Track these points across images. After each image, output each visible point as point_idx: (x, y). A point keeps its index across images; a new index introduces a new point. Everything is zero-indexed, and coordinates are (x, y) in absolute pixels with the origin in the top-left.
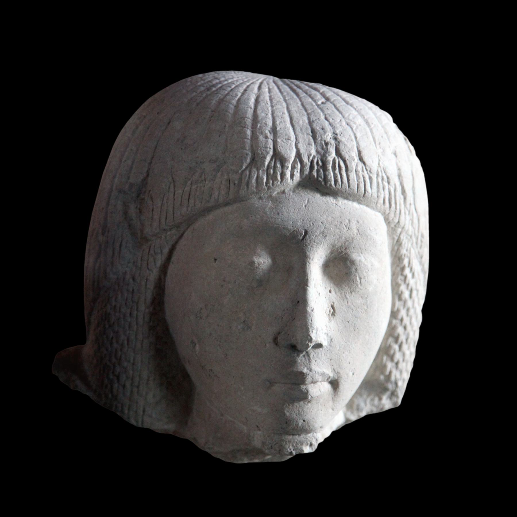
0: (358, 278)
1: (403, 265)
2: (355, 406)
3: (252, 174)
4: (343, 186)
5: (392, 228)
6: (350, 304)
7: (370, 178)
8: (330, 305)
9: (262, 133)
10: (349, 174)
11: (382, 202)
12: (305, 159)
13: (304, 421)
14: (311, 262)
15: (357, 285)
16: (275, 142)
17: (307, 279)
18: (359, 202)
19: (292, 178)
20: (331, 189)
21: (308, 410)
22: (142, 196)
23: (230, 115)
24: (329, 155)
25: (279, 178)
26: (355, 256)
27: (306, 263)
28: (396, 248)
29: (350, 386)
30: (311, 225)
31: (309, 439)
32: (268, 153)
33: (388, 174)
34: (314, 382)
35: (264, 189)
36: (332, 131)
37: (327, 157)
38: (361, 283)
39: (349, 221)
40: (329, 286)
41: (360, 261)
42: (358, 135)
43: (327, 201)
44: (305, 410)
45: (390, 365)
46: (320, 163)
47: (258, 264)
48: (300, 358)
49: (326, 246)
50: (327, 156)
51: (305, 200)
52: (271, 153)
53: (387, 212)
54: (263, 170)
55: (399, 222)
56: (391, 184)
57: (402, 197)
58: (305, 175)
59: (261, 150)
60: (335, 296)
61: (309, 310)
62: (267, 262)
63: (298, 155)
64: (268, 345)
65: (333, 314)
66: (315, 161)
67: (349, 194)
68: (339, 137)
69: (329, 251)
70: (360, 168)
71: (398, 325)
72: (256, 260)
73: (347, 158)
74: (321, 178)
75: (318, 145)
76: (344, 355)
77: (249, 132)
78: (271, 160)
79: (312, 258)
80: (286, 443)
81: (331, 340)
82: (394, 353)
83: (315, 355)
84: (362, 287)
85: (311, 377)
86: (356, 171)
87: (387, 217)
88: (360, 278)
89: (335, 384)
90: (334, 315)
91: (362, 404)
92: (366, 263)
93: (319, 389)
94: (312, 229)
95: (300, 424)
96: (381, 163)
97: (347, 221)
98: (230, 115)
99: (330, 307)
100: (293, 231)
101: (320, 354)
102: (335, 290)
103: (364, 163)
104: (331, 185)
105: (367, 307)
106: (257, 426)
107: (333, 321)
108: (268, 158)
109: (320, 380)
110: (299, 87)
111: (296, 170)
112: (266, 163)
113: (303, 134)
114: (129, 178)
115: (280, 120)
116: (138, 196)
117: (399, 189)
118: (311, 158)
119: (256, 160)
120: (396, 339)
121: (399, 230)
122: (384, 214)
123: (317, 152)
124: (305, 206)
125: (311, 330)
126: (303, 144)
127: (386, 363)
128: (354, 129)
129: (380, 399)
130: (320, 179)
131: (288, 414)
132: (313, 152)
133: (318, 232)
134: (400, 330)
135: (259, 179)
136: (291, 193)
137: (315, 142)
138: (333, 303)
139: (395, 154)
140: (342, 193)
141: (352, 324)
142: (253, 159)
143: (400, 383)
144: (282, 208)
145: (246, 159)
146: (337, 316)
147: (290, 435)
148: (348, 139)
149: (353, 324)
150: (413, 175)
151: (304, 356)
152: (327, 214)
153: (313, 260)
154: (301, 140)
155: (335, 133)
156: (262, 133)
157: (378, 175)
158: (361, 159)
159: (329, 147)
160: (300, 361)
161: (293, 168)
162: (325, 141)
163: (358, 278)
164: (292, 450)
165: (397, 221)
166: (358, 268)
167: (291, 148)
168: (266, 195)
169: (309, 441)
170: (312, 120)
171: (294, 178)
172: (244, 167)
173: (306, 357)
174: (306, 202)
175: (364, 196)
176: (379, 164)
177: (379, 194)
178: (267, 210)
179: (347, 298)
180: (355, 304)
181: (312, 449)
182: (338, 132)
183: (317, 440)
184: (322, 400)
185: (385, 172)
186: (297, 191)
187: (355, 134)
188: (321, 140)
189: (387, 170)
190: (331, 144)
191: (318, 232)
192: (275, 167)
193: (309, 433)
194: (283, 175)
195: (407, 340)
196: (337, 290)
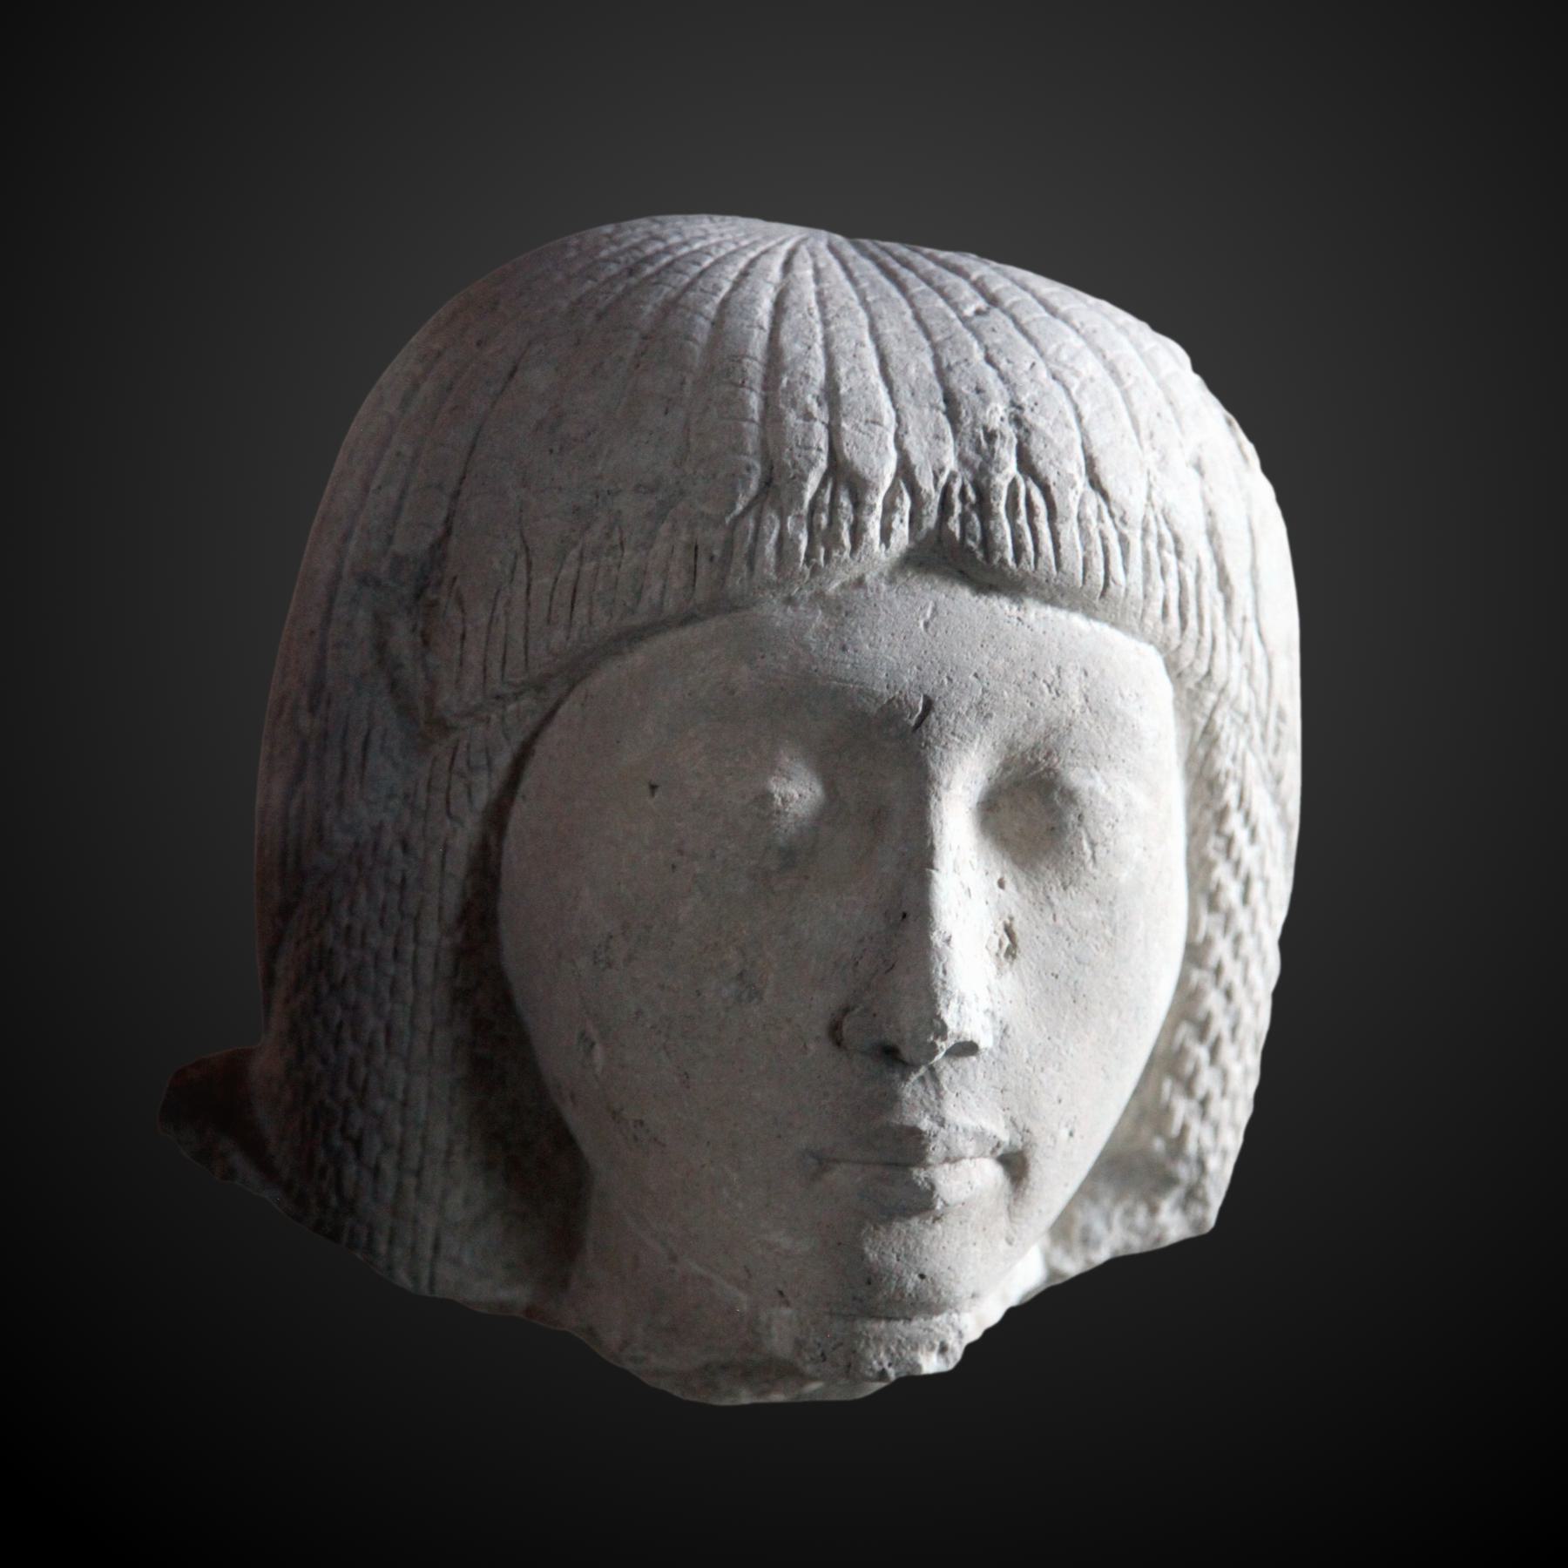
0: (1085, 844)
1: (1222, 804)
2: (1076, 1233)
3: (766, 528)
4: (1041, 565)
5: (1190, 691)
6: (1060, 921)
7: (1123, 540)
8: (1000, 924)
9: (794, 404)
10: (1060, 527)
11: (1159, 612)
12: (926, 483)
13: (922, 1276)
14: (944, 794)
15: (1083, 863)
16: (834, 431)
17: (932, 847)
18: (1090, 612)
19: (885, 540)
20: (1004, 574)
21: (935, 1245)
22: (430, 595)
23: (698, 350)
24: (998, 471)
25: (846, 539)
26: (1075, 777)
27: (928, 798)
28: (1201, 752)
29: (1062, 1172)
30: (942, 684)
31: (937, 1330)
32: (812, 464)
33: (1176, 529)
34: (952, 1159)
35: (802, 574)
36: (1007, 398)
37: (990, 477)
38: (1093, 857)
39: (1059, 669)
40: (999, 866)
41: (1092, 791)
42: (1086, 410)
43: (992, 610)
44: (925, 1243)
45: (1182, 1108)
46: (971, 495)
47: (784, 800)
48: (909, 1085)
49: (989, 747)
50: (993, 472)
51: (926, 606)
52: (823, 464)
53: (1175, 642)
54: (799, 516)
55: (1209, 673)
56: (1185, 557)
57: (1219, 597)
58: (924, 530)
59: (791, 456)
60: (1017, 897)
61: (937, 939)
62: (808, 794)
63: (905, 471)
64: (812, 1047)
65: (1011, 953)
66: (956, 488)
67: (1058, 588)
68: (1028, 415)
69: (997, 762)
70: (1090, 511)
71: (1209, 986)
72: (777, 787)
73: (1053, 478)
74: (974, 539)
75: (966, 439)
76: (1043, 1077)
77: (754, 401)
78: (823, 484)
79: (945, 782)
80: (867, 1345)
81: (1005, 1031)
82: (1196, 1072)
83: (956, 1078)
84: (1097, 872)
85: (944, 1143)
86: (1079, 520)
87: (1173, 658)
88: (1093, 844)
89: (1015, 1165)
90: (1014, 956)
91: (1098, 1226)
92: (1110, 799)
93: (966, 1180)
94: (947, 694)
95: (910, 1285)
96: (1154, 494)
97: (1053, 671)
98: (698, 350)
99: (1001, 932)
100: (890, 701)
101: (970, 1073)
102: (1015, 879)
103: (1104, 495)
104: (1003, 561)
105: (1114, 932)
106: (781, 1293)
107: (1009, 975)
108: (814, 480)
109: (970, 1152)
110: (907, 265)
111: (897, 516)
112: (808, 496)
113: (919, 406)
114: (390, 539)
115: (849, 364)
116: (419, 594)
117: (1210, 572)
118: (943, 480)
119: (777, 485)
120: (1202, 1028)
121: (1211, 698)
122: (1163, 648)
123: (963, 460)
124: (926, 625)
125: (942, 1001)
126: (918, 437)
127: (1169, 1102)
128: (1073, 391)
129: (1153, 1210)
130: (971, 543)
131: (873, 1256)
132: (951, 462)
133: (966, 703)
134: (1213, 1001)
135: (784, 544)
136: (884, 587)
137: (955, 432)
138: (1011, 919)
139: (1199, 467)
140: (1038, 585)
141: (1066, 984)
142: (767, 483)
143: (1213, 1163)
144: (855, 631)
145: (746, 482)
146: (1022, 960)
147: (879, 1318)
148: (1056, 421)
149: (1071, 983)
150: (1251, 531)
151: (922, 1079)
152: (992, 650)
153: (948, 788)
154: (912, 425)
155: (1015, 404)
156: (794, 404)
157: (1145, 530)
158: (1095, 483)
159: (997, 445)
160: (909, 1095)
161: (890, 508)
162: (985, 428)
163: (1085, 844)
164: (886, 1365)
165: (1203, 669)
166: (1087, 813)
167: (882, 449)
168: (807, 593)
169: (938, 1336)
170: (945, 364)
171: (892, 540)
172: (740, 508)
173: (928, 1081)
174: (929, 612)
175: (1103, 594)
176: (1149, 498)
177: (1150, 589)
178: (809, 636)
179: (1052, 905)
180: (1075, 923)
181: (947, 1361)
182: (1024, 399)
183: (961, 1335)
184: (975, 1214)
185: (1167, 522)
186: (901, 580)
187: (1076, 408)
188: (974, 424)
189: (1173, 515)
190: (1003, 437)
191: (966, 703)
192: (834, 506)
193: (938, 1312)
194: (857, 531)
195: (1234, 1030)
196: (1022, 879)
